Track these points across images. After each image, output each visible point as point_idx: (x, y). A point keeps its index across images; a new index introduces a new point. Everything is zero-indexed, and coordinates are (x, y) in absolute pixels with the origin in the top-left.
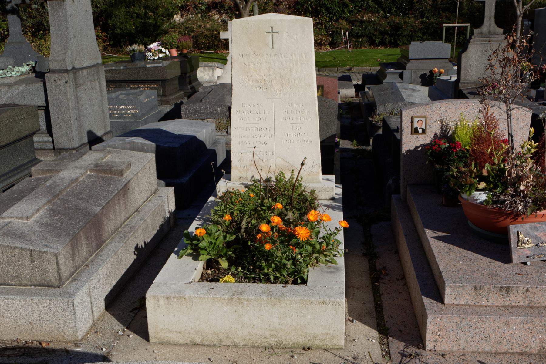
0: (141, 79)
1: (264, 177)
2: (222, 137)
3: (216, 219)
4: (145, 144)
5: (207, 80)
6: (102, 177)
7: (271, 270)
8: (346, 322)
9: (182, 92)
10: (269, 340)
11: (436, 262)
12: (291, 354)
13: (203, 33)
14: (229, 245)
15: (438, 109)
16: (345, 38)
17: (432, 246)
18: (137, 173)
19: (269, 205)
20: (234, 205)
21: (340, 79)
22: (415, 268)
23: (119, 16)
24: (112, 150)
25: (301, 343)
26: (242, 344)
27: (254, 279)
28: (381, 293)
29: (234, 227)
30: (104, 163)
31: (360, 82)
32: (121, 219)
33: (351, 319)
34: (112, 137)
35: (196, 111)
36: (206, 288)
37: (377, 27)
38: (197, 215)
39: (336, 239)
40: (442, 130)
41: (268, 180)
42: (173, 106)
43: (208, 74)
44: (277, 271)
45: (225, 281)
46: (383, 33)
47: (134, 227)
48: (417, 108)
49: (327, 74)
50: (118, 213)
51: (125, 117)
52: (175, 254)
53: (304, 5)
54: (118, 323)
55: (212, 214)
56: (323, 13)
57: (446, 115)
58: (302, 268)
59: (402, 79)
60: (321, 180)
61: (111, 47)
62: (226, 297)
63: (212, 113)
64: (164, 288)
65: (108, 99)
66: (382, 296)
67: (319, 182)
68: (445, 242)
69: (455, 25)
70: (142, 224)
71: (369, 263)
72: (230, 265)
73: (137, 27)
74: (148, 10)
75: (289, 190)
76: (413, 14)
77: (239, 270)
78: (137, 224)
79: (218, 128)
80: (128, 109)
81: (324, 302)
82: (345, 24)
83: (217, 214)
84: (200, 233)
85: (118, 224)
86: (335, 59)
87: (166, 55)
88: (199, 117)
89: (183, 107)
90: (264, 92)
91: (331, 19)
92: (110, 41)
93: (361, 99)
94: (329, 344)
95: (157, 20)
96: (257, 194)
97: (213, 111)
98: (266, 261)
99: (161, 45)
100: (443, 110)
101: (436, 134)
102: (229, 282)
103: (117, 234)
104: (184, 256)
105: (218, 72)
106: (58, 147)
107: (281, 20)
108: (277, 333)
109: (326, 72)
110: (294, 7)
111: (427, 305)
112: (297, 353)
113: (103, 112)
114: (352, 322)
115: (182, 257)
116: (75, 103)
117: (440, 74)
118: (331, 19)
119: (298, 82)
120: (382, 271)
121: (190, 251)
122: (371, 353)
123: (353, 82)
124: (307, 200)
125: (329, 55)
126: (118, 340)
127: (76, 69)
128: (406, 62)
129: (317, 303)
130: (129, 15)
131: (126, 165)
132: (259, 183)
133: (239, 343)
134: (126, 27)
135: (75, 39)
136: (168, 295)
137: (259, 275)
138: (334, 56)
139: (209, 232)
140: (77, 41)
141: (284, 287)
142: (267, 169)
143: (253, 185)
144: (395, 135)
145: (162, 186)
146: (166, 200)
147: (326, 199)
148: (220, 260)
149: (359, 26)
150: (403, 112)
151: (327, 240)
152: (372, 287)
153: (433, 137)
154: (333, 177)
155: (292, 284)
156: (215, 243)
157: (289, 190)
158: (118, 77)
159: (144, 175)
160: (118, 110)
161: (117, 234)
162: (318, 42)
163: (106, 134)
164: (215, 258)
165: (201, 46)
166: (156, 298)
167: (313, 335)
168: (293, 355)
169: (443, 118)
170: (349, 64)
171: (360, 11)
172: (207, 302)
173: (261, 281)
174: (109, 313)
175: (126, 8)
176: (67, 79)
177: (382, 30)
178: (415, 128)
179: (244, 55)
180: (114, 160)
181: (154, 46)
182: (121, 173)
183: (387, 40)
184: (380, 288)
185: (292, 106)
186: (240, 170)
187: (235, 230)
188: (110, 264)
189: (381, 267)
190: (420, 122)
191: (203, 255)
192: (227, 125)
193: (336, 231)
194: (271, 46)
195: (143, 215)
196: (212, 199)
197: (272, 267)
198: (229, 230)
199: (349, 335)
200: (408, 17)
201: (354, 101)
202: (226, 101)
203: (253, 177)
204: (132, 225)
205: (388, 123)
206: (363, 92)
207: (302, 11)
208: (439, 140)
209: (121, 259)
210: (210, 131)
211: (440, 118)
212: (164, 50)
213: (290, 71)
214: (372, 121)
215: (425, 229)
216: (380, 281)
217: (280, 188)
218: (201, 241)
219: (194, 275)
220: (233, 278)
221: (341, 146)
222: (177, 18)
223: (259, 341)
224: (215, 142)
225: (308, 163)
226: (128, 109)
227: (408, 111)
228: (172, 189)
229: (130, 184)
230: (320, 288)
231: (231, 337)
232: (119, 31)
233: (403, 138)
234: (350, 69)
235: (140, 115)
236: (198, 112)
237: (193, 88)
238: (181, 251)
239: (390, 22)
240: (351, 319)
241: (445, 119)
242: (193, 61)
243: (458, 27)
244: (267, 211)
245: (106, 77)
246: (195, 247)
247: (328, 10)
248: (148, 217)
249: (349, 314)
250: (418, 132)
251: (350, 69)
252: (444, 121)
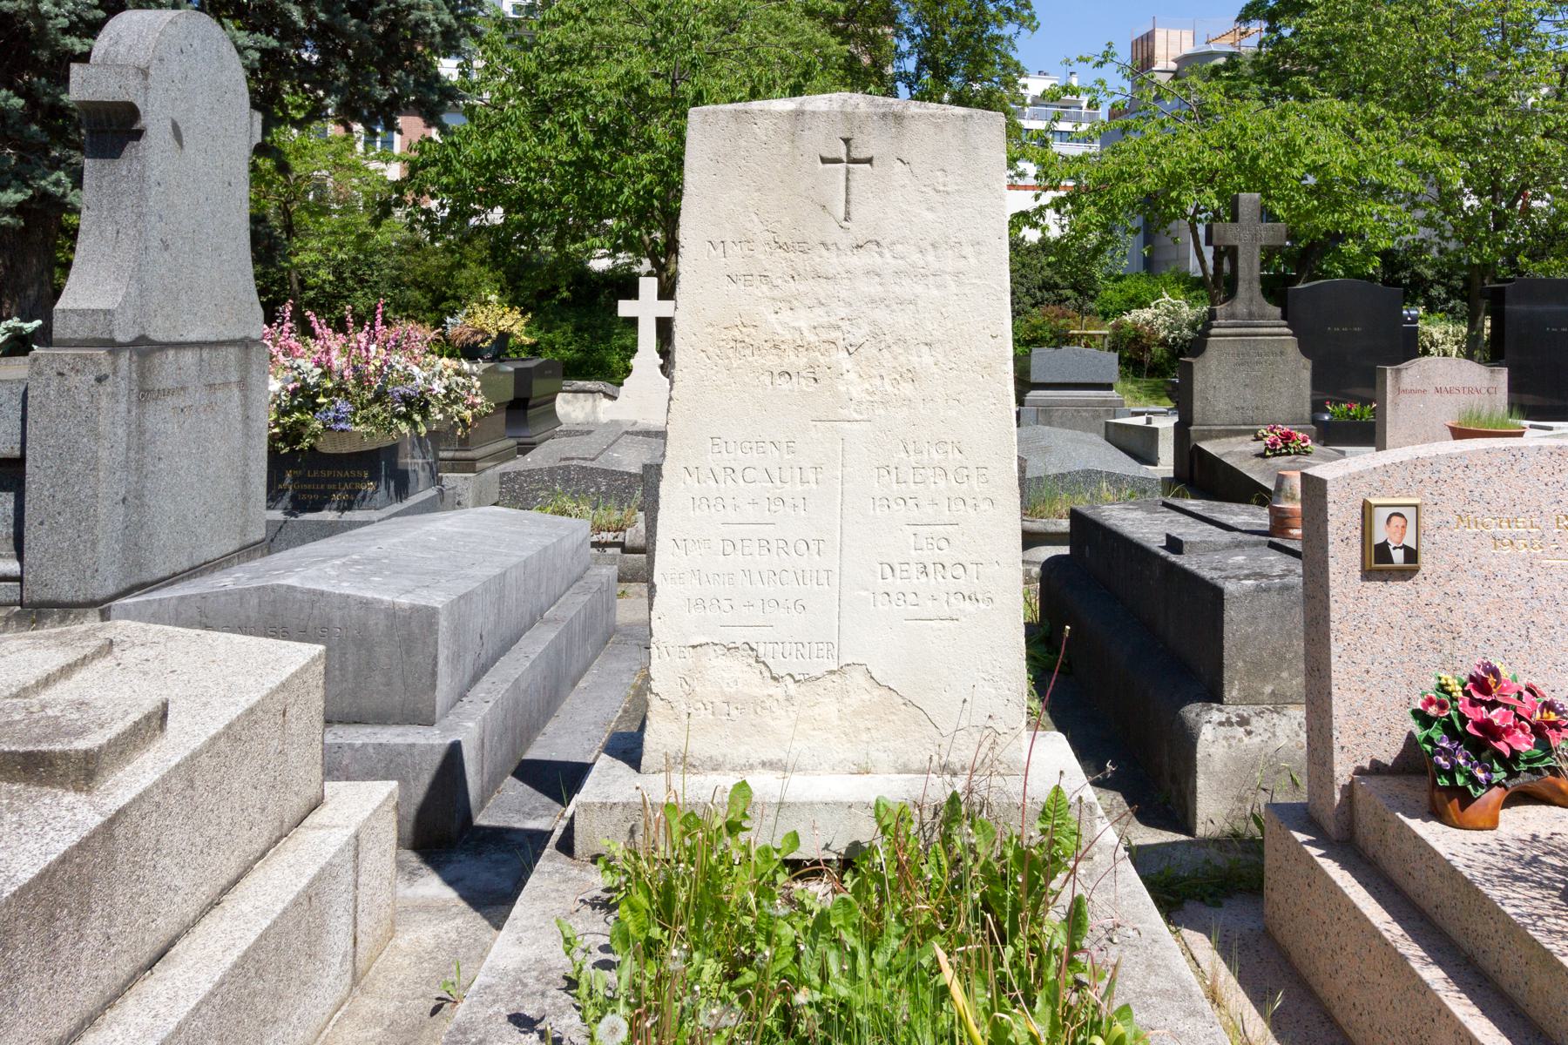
15: (1459, 471)
43: (583, 408)
106: (36, 598)
116: (128, 449)
127: (152, 343)
135: (166, 255)
140: (175, 259)
160: (317, 481)
176: (106, 369)
178: (1377, 547)
194: (842, 215)
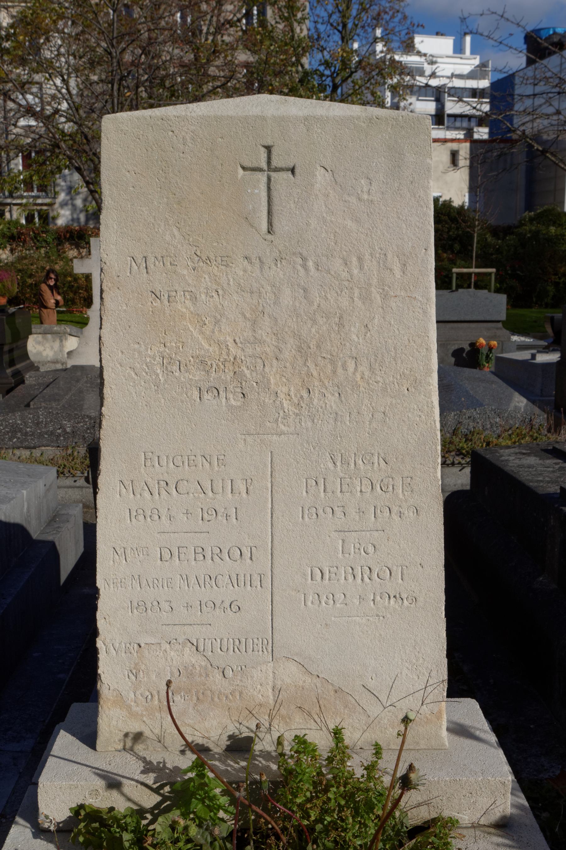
5: (49, 359)
35: (14, 430)
43: (52, 348)
63: (52, 433)
69: (471, 270)
88: (21, 442)
90: (230, 407)
105: (72, 343)
107: (306, 119)
119: (371, 369)
179: (151, 260)
185: (345, 462)
186: (134, 709)
194: (264, 226)
202: (85, 406)
213: (341, 325)
236: (20, 430)
243: (477, 274)
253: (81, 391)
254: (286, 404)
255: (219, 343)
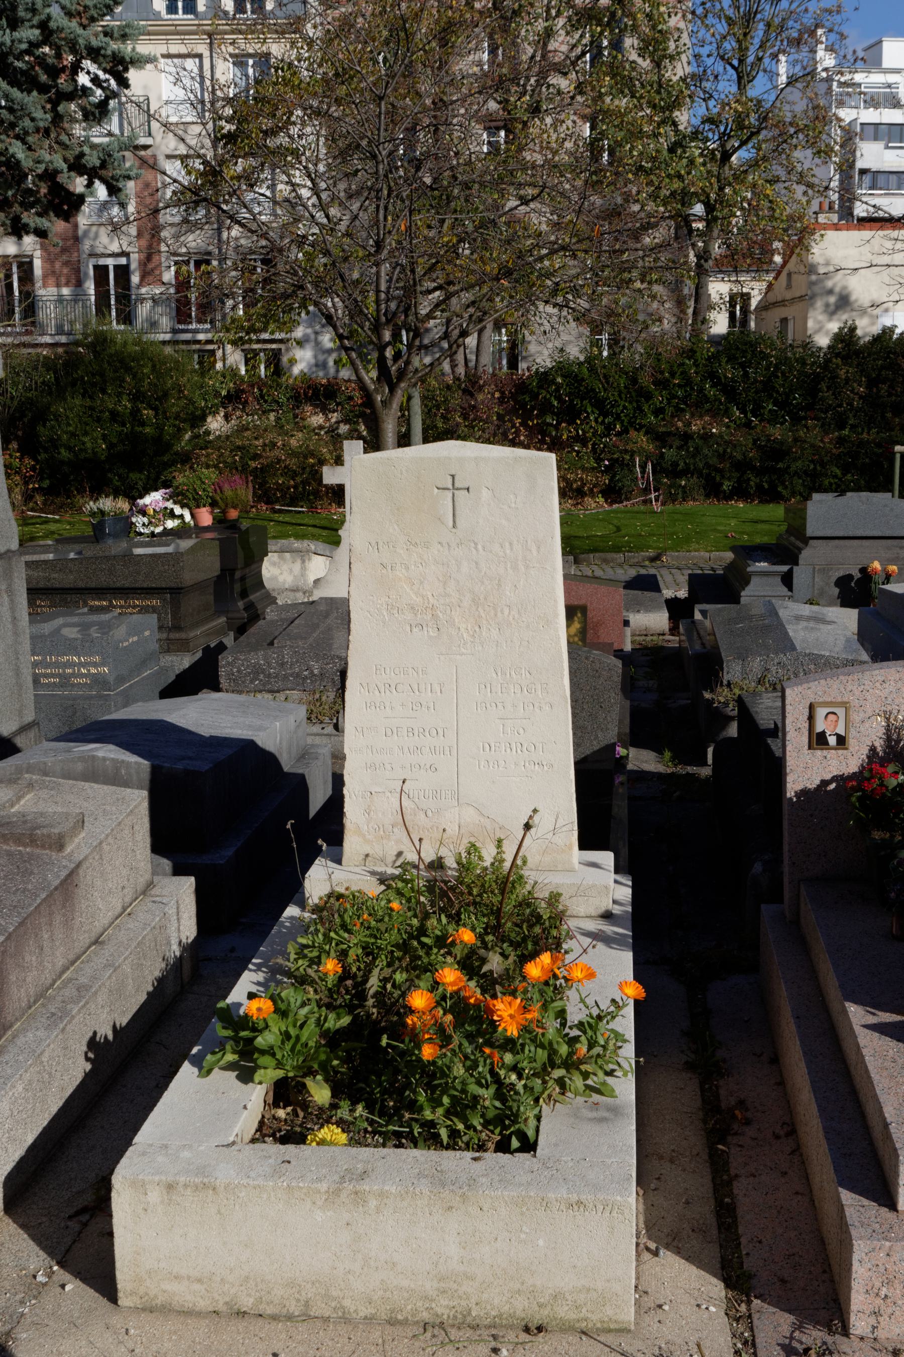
0: (118, 585)
1: (429, 856)
2: (325, 740)
3: (301, 969)
4: (123, 761)
5: (287, 586)
6: (10, 854)
7: (440, 1111)
8: (638, 1254)
9: (223, 619)
10: (434, 1305)
11: (876, 1095)
12: (493, 1344)
13: (279, 461)
14: (332, 1039)
15: (878, 684)
16: (643, 477)
17: (865, 1052)
18: (101, 843)
19: (439, 933)
20: (349, 931)
21: (630, 585)
22: (822, 1110)
23: (67, 417)
24: (36, 781)
25: (520, 1313)
26: (362, 1314)
27: (398, 1135)
28: (733, 1172)
29: (347, 992)
30: (14, 815)
31: (683, 594)
32: (53, 966)
33: (652, 1246)
34: (37, 741)
35: (257, 671)
36: (271, 1161)
37: (725, 451)
38: (253, 957)
39: (612, 1031)
40: (888, 738)
41: (438, 865)
42: (199, 655)
44: (457, 1115)
45: (321, 1143)
46: (742, 466)
47: (87, 988)
48: (823, 682)
49: (599, 573)
50: (47, 950)
51: (73, 685)
52: (193, 1064)
53: (538, 394)
54: (37, 1248)
55: (293, 956)
56: (588, 414)
57: (897, 702)
58: (522, 1109)
59: (790, 589)
60: (577, 866)
61: (44, 495)
62: (323, 1187)
63: (298, 675)
64: (160, 1159)
65: (32, 638)
66: (735, 1183)
67: (572, 870)
68: (899, 1040)
70: (110, 977)
71: (702, 1090)
72: (336, 1093)
73: (111, 446)
74: (143, 402)
75: (492, 892)
76: (817, 419)
77: (357, 1114)
78: (94, 978)
79: (313, 716)
80: (81, 665)
81: (579, 1203)
82: (641, 440)
83: (305, 956)
84: (259, 1009)
85: (47, 977)
86: (618, 529)
87: (184, 521)
88: (264, 685)
89: (224, 660)
91: (609, 428)
92: (42, 480)
93: (683, 638)
94: (594, 1317)
95: (163, 429)
96: (409, 900)
97: (301, 671)
98: (430, 1087)
99: (171, 497)
100: (890, 687)
101: (873, 749)
102: (331, 1143)
103: (43, 1005)
104: (216, 1070)
105: (317, 566)
107: (476, 458)
108: (455, 1286)
109: (594, 567)
110: (513, 396)
111: (851, 1213)
112: (509, 1342)
113: (18, 673)
114: (656, 1253)
115: (209, 1072)
117: (888, 578)
118: (609, 428)
119: (519, 612)
120: (737, 1112)
121: (230, 1057)
122: (705, 1344)
123: (664, 592)
124: (539, 917)
125: (603, 520)
126: (35, 1297)
128: (800, 545)
129: (563, 1207)
130: (91, 416)
131: (72, 821)
132: (415, 872)
133: (355, 1311)
134: (84, 443)
136: (170, 1179)
137: (410, 1126)
138: (615, 522)
139: (283, 1006)
141: (475, 1159)
142: (437, 835)
143: (400, 878)
144: (768, 747)
145: (165, 875)
146: (172, 911)
147: (590, 917)
148: (309, 1082)
149: (680, 448)
150: (788, 692)
151: (590, 1033)
152: (711, 1156)
153: (864, 757)
154: (607, 858)
155: (495, 1152)
156: (298, 1038)
157: (492, 892)
158: (59, 579)
159: (119, 848)
161: (43, 1005)
162: (575, 486)
163: (24, 729)
164: (296, 1076)
165: (275, 494)
166: (139, 1186)
167: (550, 1291)
168: (499, 1346)
169: (889, 708)
170: (654, 545)
171: (683, 410)
172: (273, 1199)
173: (415, 1143)
174: (14, 1222)
175: (83, 396)
177: (739, 457)
178: (818, 734)
179: (381, 544)
180: (42, 807)
181: (154, 499)
182: (59, 844)
183: (752, 483)
184: (732, 1159)
186: (368, 837)
187: (351, 1000)
188: (20, 1088)
189: (733, 1101)
190: (831, 717)
191: (265, 1068)
192: (337, 707)
193: (612, 1009)
194: (451, 523)
195: (112, 955)
196: (292, 911)
197: (442, 1105)
198: (336, 1000)
199: (646, 1293)
200: (806, 426)
201: (665, 644)
202: (335, 646)
203: (400, 854)
204: (83, 980)
205: (752, 710)
206: (689, 620)
207: (533, 408)
208: (882, 766)
209: (50, 1074)
210: (292, 725)
211: (883, 708)
212: (178, 510)
213: (499, 585)
214: (712, 701)
215: (847, 1004)
216: (729, 1138)
217: (468, 886)
218: (261, 1031)
219: (239, 1125)
220: (343, 1131)
221: (630, 767)
222: (216, 424)
223: (409, 1307)
224: (305, 755)
225: (543, 823)
226: (81, 665)
227: (800, 688)
228: (188, 883)
229: (84, 866)
230: (571, 1164)
231: (334, 1294)
232: (64, 454)
233: (788, 753)
234: (656, 559)
235: (111, 679)
237: (250, 607)
238: (209, 1057)
239: (759, 439)
240: (652, 1246)
241: (895, 712)
242: (252, 539)
244: (435, 950)
245: (28, 581)
246: (244, 1045)
247: (600, 405)
248: (125, 959)
249: (647, 1231)
250: (827, 743)
251: (656, 559)
252: (893, 717)
253: (329, 629)
254: (465, 635)
255: (423, 597)
